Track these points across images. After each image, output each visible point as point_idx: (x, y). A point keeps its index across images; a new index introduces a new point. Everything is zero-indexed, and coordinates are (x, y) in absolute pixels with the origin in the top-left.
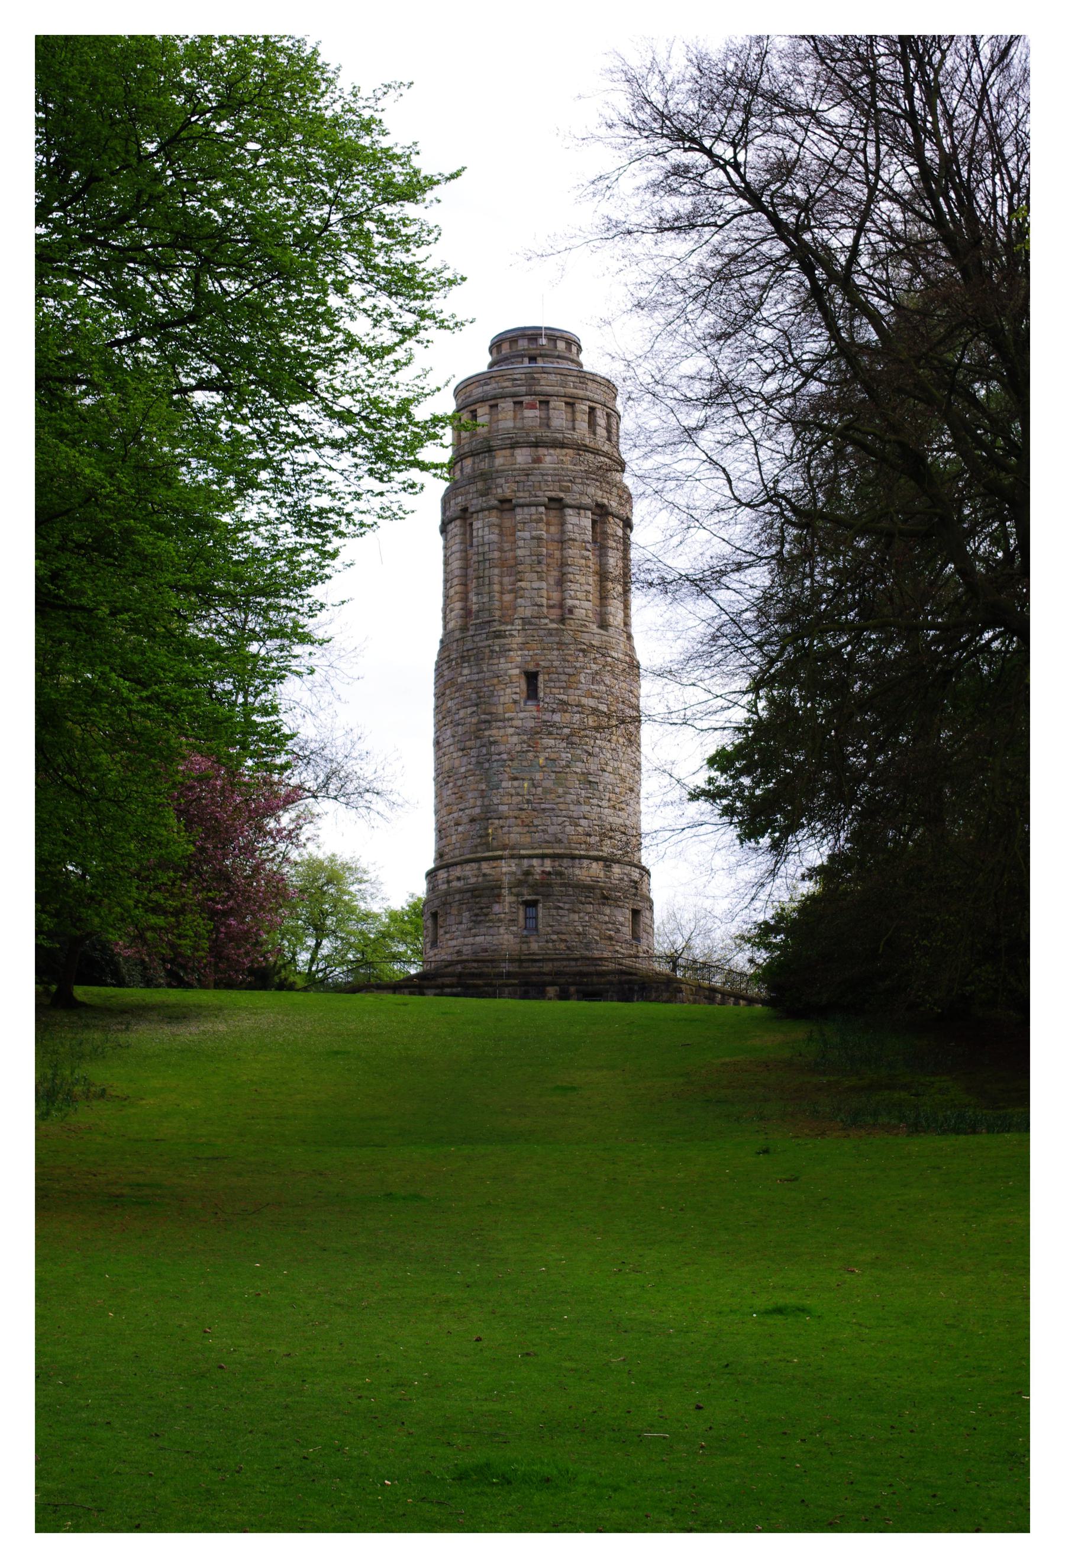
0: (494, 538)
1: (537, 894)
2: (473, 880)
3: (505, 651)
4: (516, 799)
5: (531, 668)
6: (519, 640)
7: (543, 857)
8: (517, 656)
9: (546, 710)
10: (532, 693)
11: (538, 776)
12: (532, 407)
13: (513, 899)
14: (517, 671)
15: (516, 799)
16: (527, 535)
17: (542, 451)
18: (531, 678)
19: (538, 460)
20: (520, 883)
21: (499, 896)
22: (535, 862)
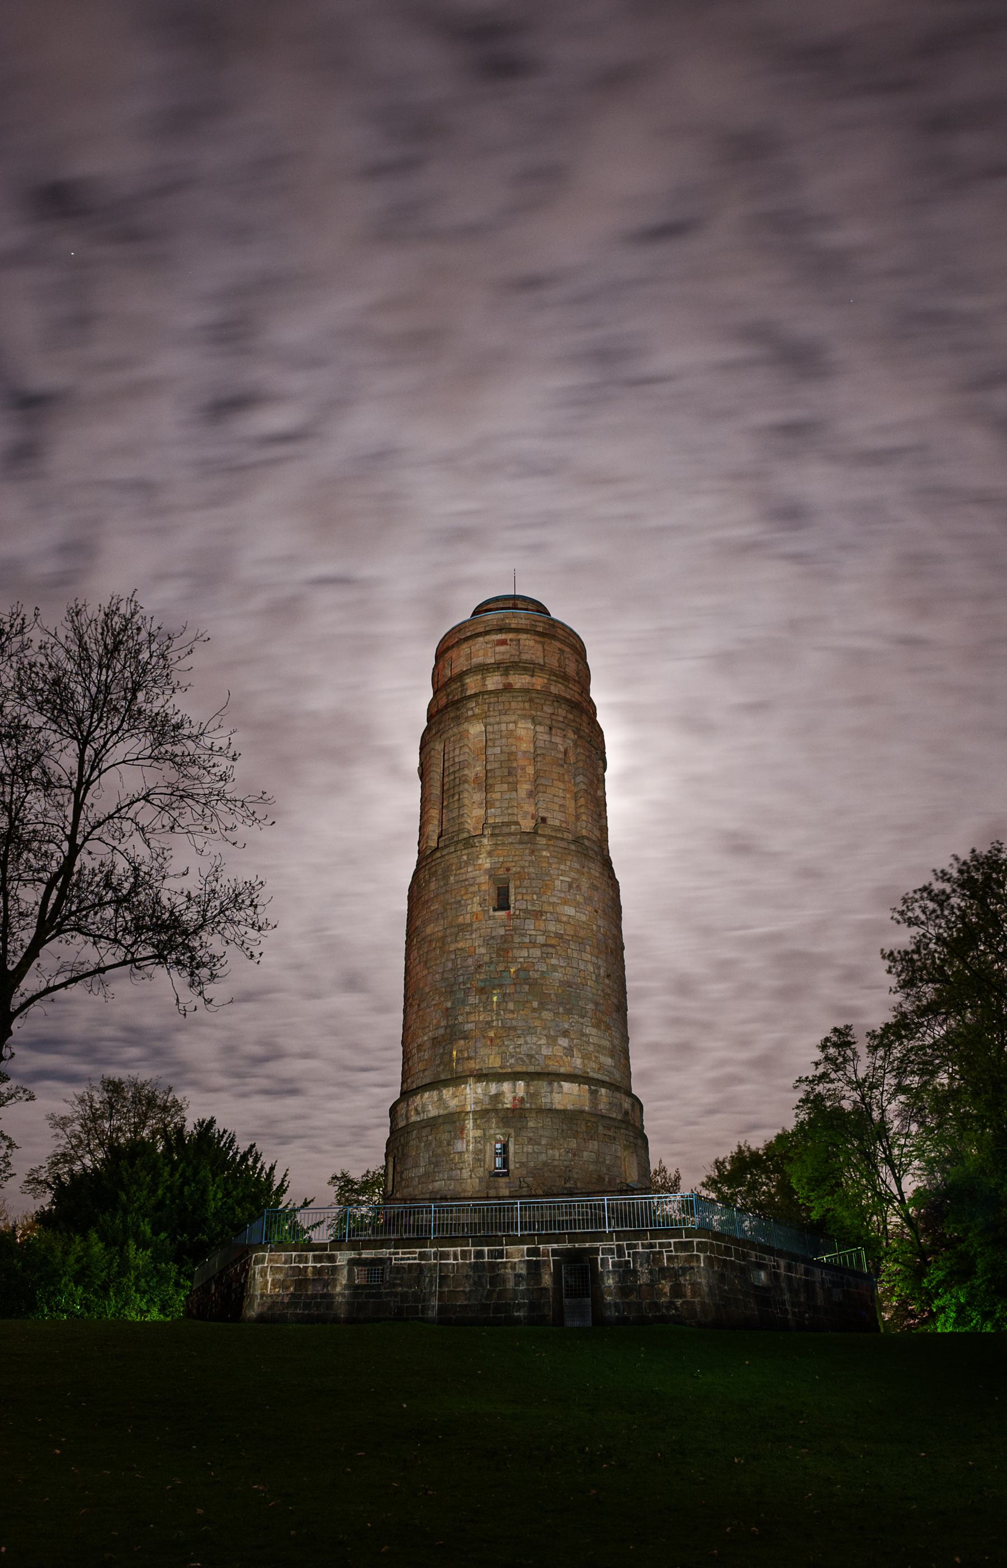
1: (509, 1127)
9: (518, 917)
13: (479, 1133)
16: (497, 750)
21: (463, 1129)
22: (506, 1086)
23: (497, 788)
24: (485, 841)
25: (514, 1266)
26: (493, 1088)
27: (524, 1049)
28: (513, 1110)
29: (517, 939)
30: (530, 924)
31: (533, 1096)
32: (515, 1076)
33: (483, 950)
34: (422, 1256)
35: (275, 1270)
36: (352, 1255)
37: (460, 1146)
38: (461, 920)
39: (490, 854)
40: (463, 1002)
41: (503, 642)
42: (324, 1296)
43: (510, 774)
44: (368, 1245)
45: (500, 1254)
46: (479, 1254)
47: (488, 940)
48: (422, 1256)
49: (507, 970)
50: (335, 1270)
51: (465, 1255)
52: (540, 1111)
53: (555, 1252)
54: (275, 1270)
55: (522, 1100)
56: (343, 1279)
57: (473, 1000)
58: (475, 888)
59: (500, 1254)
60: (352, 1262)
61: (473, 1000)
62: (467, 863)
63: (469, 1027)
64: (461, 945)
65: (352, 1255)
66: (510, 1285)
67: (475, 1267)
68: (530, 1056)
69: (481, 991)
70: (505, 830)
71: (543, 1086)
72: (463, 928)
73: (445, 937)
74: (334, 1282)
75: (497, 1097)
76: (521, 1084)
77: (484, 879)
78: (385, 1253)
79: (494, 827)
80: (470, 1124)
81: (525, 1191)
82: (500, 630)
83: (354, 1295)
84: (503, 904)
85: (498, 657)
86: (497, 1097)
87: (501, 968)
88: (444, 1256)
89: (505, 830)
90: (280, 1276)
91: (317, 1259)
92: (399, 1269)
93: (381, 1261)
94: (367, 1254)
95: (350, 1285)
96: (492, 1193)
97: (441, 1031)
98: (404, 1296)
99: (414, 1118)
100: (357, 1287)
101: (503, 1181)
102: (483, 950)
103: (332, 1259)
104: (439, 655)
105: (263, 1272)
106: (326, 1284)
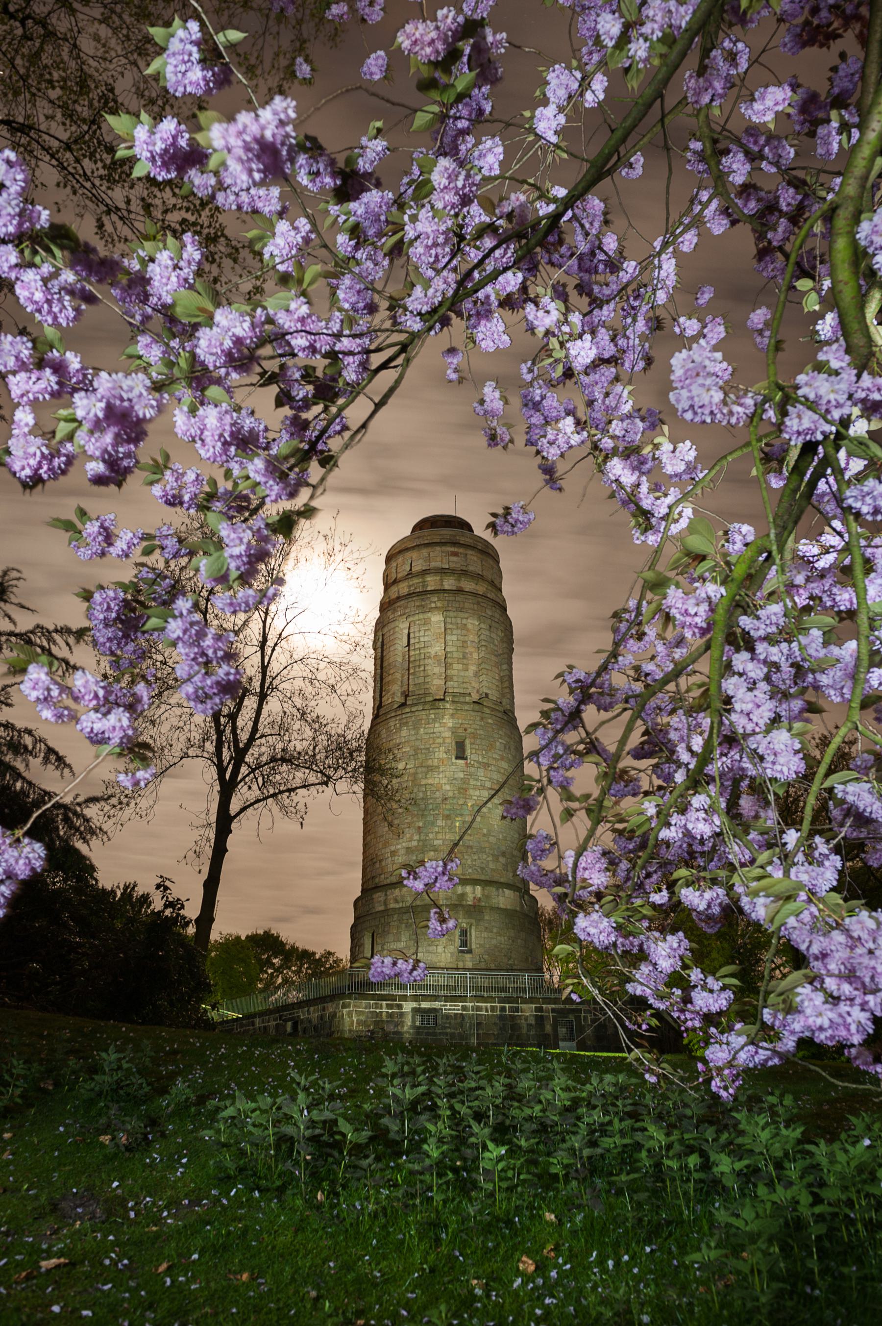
22: (469, 889)
23: (455, 666)
24: (448, 706)
25: (526, 1018)
27: (478, 863)
28: (474, 906)
29: (472, 782)
31: (488, 897)
32: (474, 882)
33: (448, 787)
34: (464, 1008)
35: (359, 1013)
36: (415, 1005)
38: (430, 762)
39: (452, 715)
40: (433, 823)
41: (455, 554)
42: (395, 1033)
43: (464, 657)
44: (425, 998)
45: (517, 1010)
46: (503, 1009)
47: (452, 780)
48: (464, 1008)
49: (465, 804)
50: (402, 1015)
51: (493, 1009)
52: (492, 908)
53: (553, 1010)
54: (359, 1013)
55: (479, 900)
56: (408, 1021)
57: (440, 823)
58: (440, 741)
59: (517, 1010)
60: (415, 1011)
61: (440, 823)
62: (434, 720)
63: (436, 842)
64: (430, 781)
65: (415, 1005)
66: (524, 1031)
67: (501, 1017)
68: (482, 868)
69: (447, 817)
70: (462, 699)
71: (492, 890)
72: (431, 769)
73: (416, 774)
74: (402, 1023)
75: (463, 896)
76: (478, 888)
77: (447, 734)
78: (437, 1005)
79: (454, 695)
81: (483, 966)
82: (454, 544)
83: (418, 1033)
85: (452, 565)
86: (463, 896)
87: (461, 802)
88: (479, 1009)
89: (462, 699)
90: (362, 1018)
91: (389, 1006)
92: (448, 1016)
93: (435, 1010)
94: (425, 1005)
95: (413, 1026)
96: (461, 965)
97: (415, 843)
98: (453, 1036)
99: (392, 905)
100: (418, 1028)
101: (468, 956)
102: (448, 787)
103: (400, 1007)
104: (389, 559)
105: (350, 1014)
106: (397, 1025)
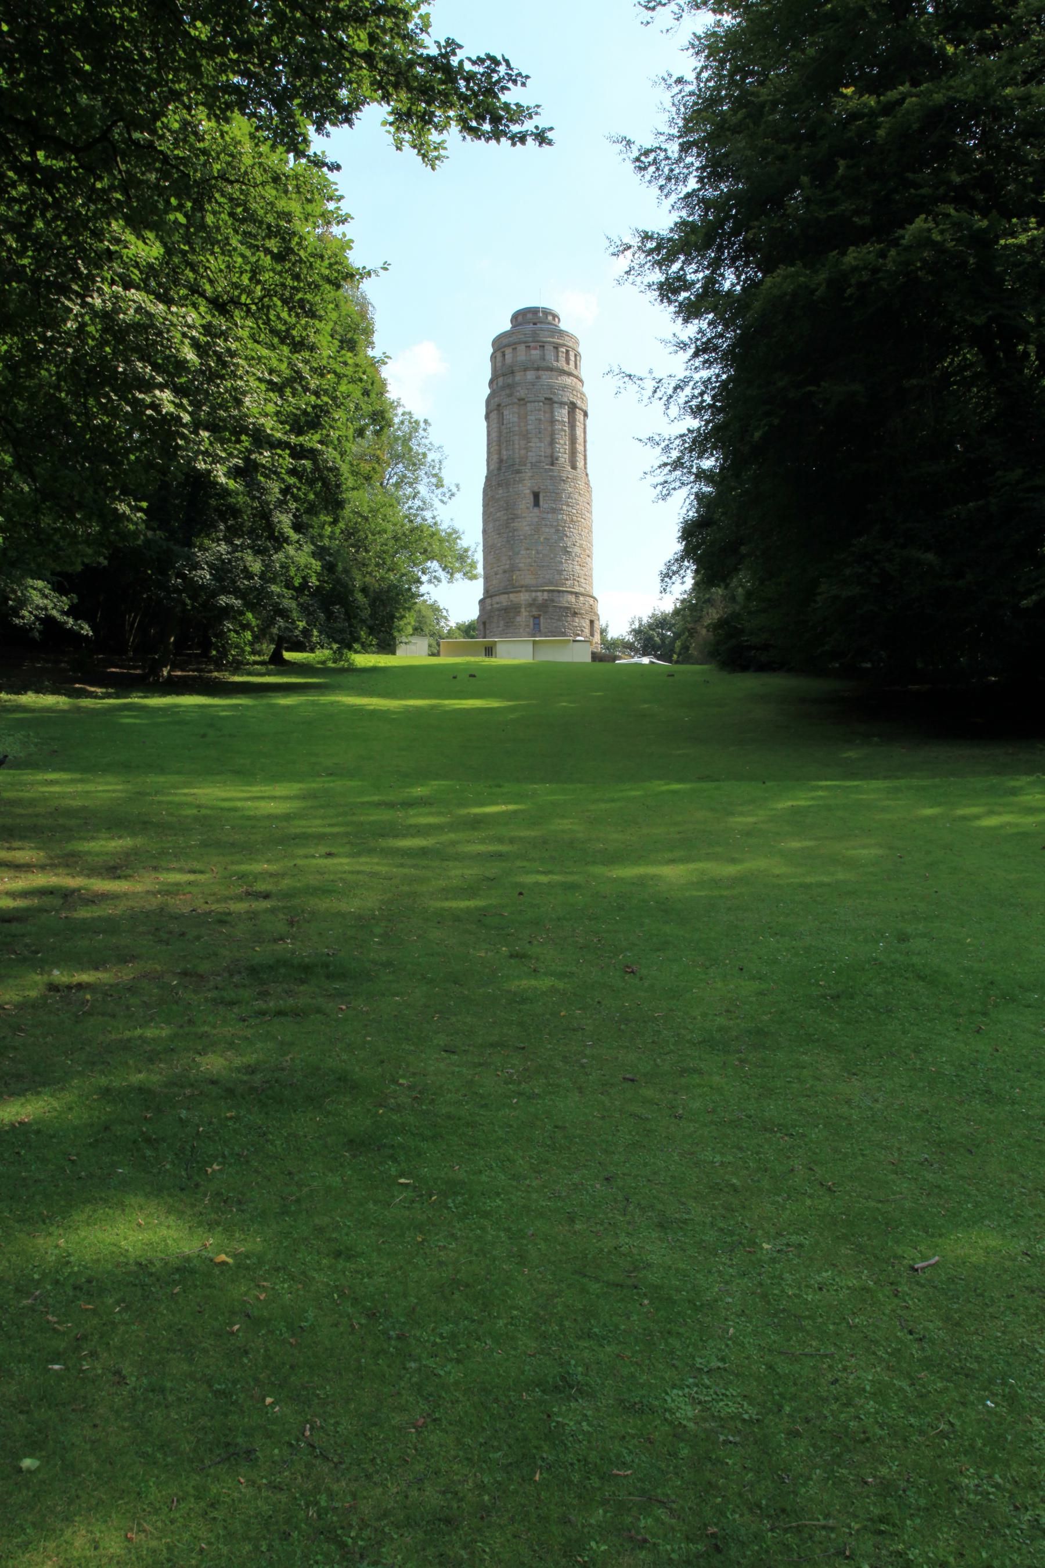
0: (516, 419)
2: (505, 604)
3: (521, 480)
4: (529, 560)
5: (536, 489)
6: (529, 474)
7: (544, 591)
8: (528, 483)
10: (537, 503)
11: (540, 548)
12: (535, 348)
14: (528, 491)
15: (529, 560)
16: (533, 418)
17: (541, 373)
18: (536, 496)
19: (538, 378)
20: (531, 605)
22: (539, 594)
26: (534, 594)
30: (550, 516)
37: (518, 619)
75: (535, 600)
80: (523, 610)
84: (537, 503)
